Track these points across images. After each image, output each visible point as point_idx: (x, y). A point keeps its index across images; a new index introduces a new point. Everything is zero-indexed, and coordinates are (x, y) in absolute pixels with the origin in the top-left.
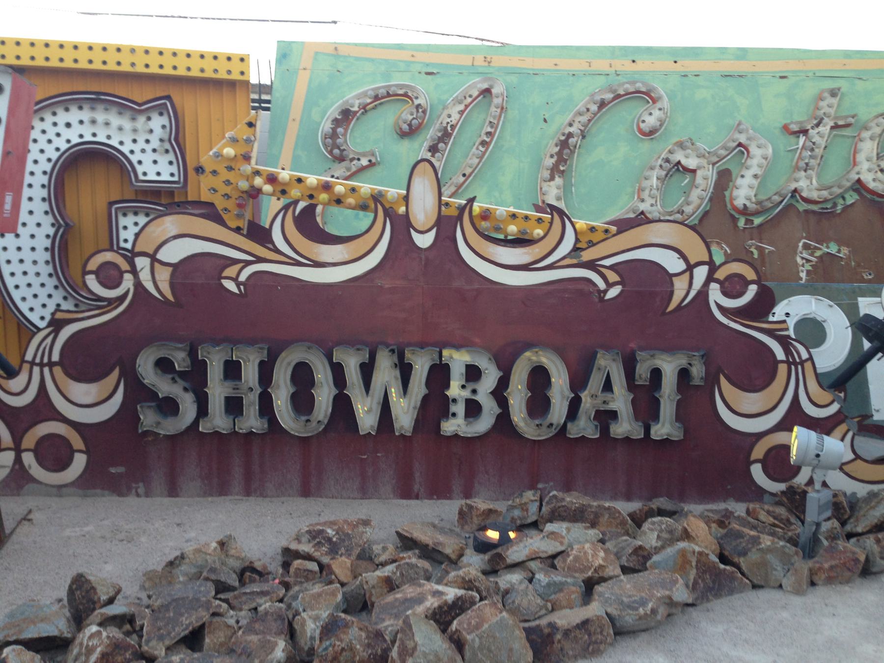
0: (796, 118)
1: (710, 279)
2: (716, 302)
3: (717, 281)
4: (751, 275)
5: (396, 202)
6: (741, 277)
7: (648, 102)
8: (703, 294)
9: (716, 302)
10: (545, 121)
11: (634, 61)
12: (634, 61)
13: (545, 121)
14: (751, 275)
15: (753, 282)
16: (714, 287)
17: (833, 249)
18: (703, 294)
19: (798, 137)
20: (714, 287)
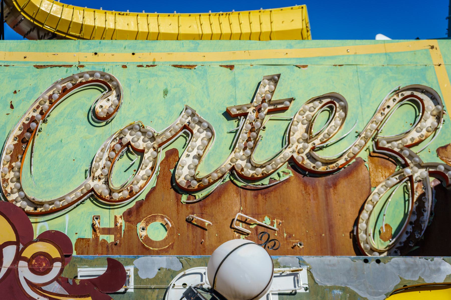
0: (239, 103)
1: (18, 257)
2: (25, 278)
3: (25, 259)
4: (55, 253)
5: (189, 172)
6: (46, 255)
7: (105, 90)
8: (12, 272)
9: (25, 278)
10: (12, 107)
11: (96, 54)
12: (96, 54)
13: (12, 107)
14: (55, 253)
15: (57, 260)
16: (22, 264)
17: (267, 222)
18: (12, 272)
19: (239, 120)
20: (22, 264)
